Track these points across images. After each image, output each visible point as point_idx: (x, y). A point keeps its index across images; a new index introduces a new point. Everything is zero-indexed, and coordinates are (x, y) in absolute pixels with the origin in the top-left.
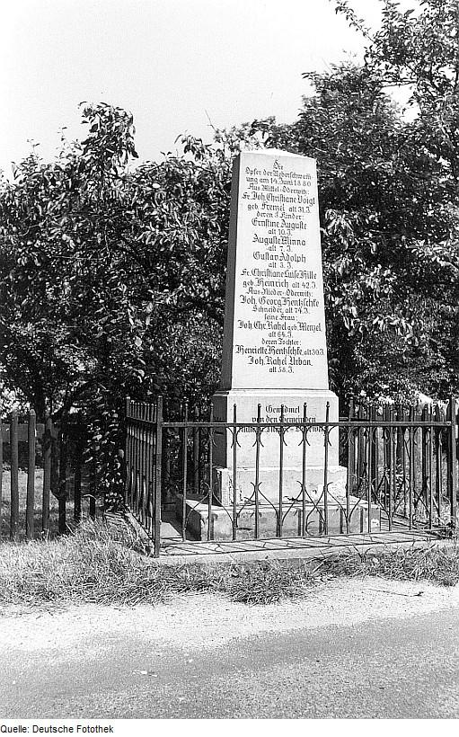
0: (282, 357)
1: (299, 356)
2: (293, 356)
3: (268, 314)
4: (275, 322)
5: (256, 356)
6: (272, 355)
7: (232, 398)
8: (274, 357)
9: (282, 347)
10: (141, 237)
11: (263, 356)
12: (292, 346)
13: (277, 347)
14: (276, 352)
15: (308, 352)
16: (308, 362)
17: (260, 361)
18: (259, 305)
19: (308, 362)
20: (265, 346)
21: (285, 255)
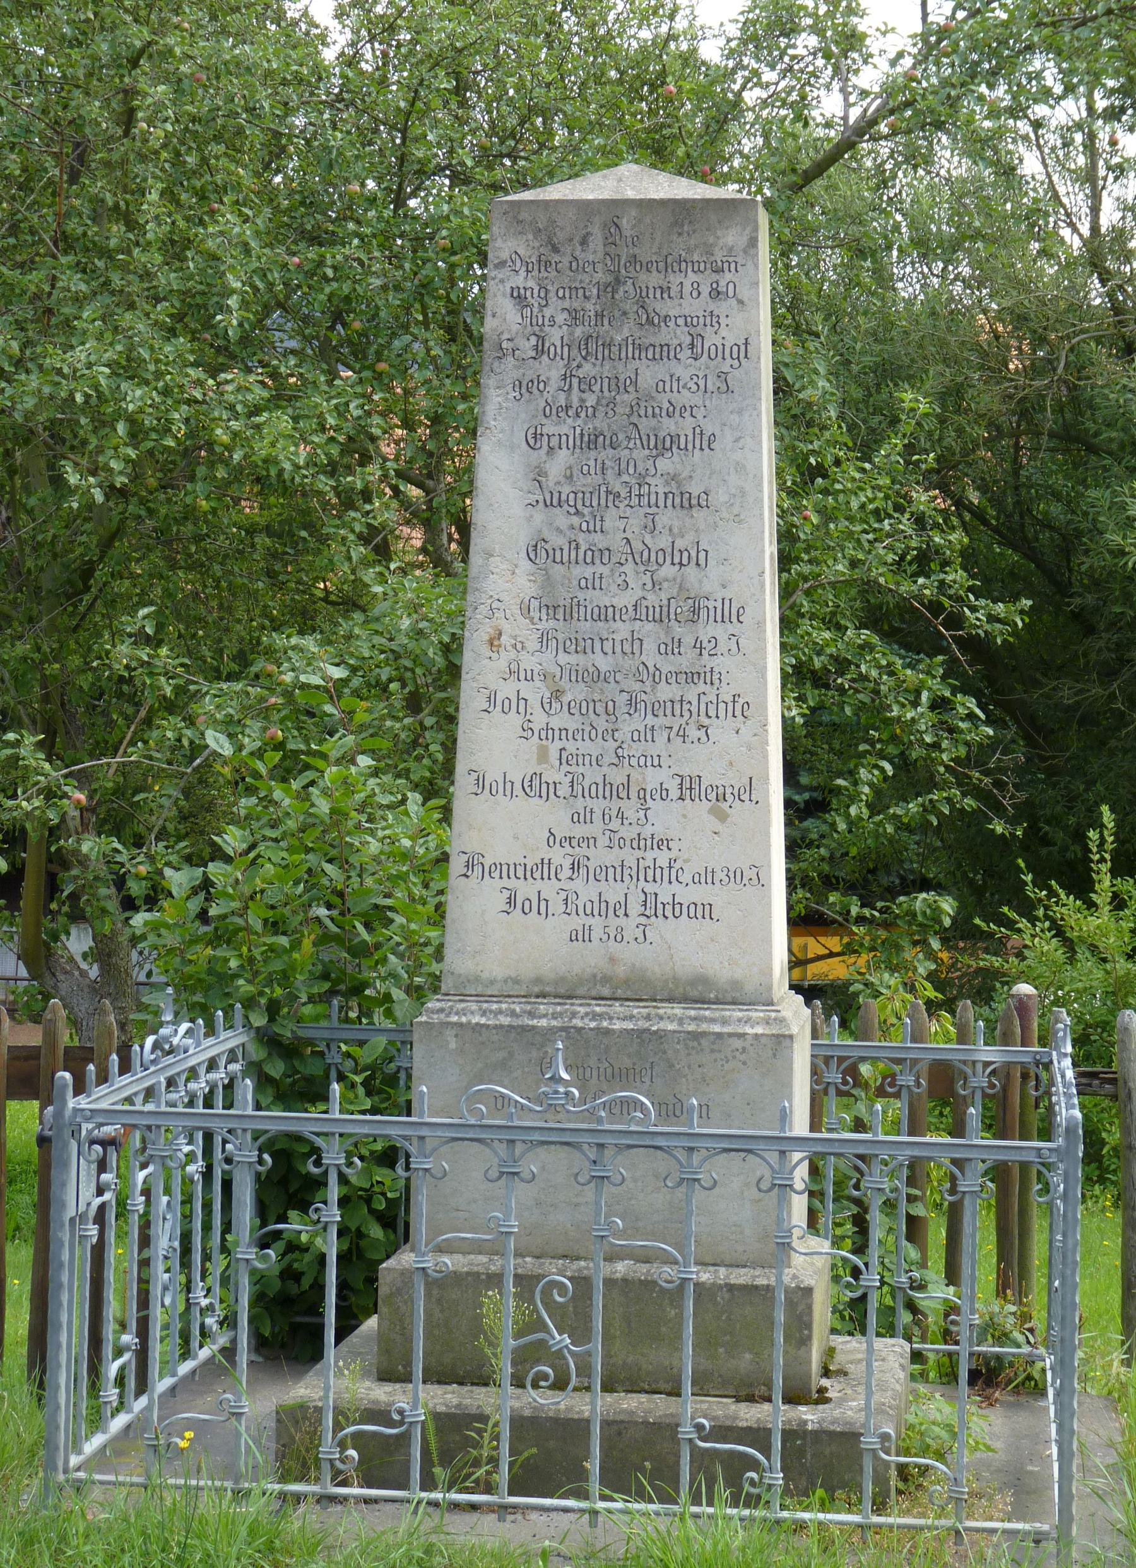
0: (614, 893)
1: (675, 887)
2: (650, 888)
3: (571, 747)
4: (592, 775)
5: (526, 890)
6: (578, 884)
7: (1119, 1220)
8: (587, 891)
9: (611, 858)
10: (119, 1422)
11: (549, 889)
12: (650, 855)
13: (600, 856)
14: (601, 874)
15: (707, 877)
16: (706, 911)
17: (542, 905)
18: (539, 719)
19: (706, 911)
20: (559, 856)
21: (637, 546)
